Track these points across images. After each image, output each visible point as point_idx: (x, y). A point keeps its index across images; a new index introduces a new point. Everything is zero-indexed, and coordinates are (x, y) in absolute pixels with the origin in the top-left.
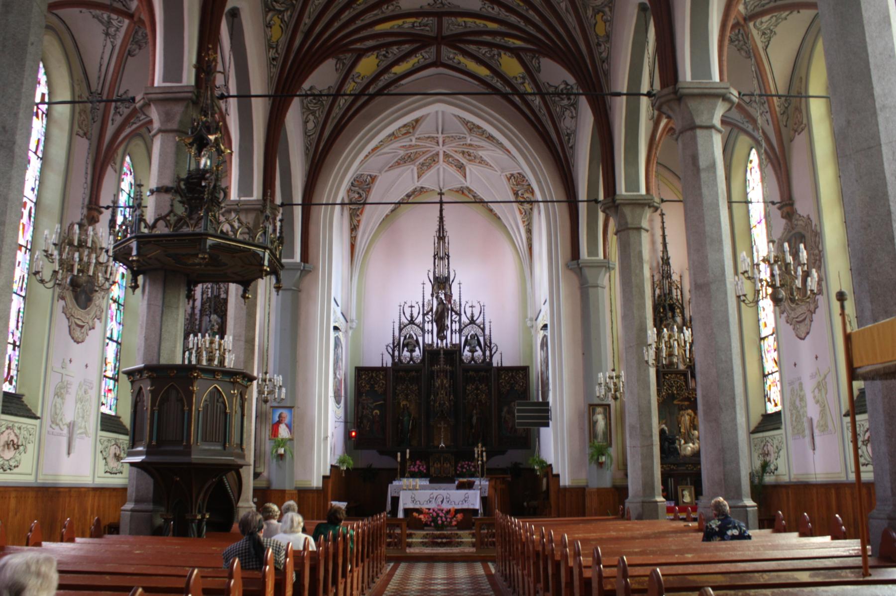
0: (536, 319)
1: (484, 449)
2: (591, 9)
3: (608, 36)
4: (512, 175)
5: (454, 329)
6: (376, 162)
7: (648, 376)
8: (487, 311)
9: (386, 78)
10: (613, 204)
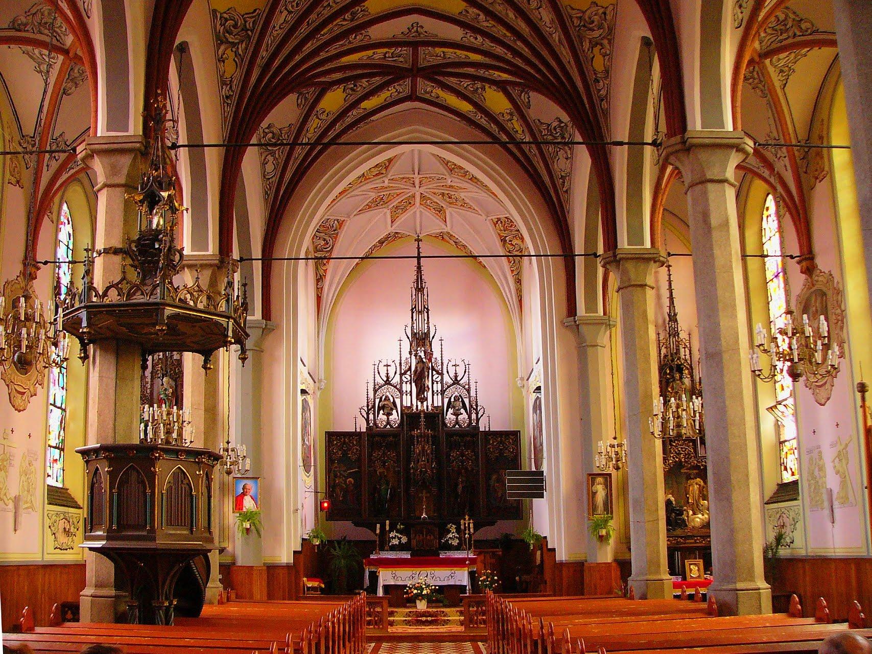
0: (528, 380)
1: (471, 521)
2: (588, 41)
3: (607, 72)
4: (499, 219)
5: (435, 389)
6: (346, 203)
7: (654, 447)
8: (472, 369)
9: (355, 114)
10: (614, 258)
